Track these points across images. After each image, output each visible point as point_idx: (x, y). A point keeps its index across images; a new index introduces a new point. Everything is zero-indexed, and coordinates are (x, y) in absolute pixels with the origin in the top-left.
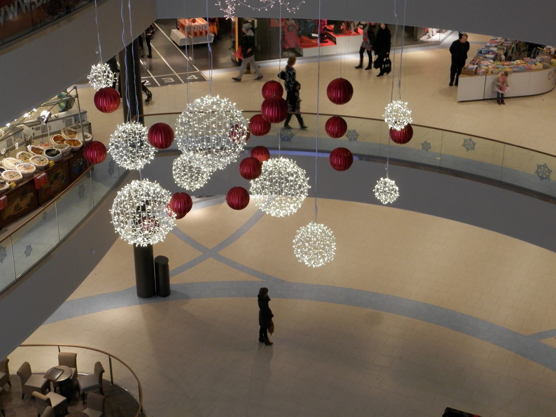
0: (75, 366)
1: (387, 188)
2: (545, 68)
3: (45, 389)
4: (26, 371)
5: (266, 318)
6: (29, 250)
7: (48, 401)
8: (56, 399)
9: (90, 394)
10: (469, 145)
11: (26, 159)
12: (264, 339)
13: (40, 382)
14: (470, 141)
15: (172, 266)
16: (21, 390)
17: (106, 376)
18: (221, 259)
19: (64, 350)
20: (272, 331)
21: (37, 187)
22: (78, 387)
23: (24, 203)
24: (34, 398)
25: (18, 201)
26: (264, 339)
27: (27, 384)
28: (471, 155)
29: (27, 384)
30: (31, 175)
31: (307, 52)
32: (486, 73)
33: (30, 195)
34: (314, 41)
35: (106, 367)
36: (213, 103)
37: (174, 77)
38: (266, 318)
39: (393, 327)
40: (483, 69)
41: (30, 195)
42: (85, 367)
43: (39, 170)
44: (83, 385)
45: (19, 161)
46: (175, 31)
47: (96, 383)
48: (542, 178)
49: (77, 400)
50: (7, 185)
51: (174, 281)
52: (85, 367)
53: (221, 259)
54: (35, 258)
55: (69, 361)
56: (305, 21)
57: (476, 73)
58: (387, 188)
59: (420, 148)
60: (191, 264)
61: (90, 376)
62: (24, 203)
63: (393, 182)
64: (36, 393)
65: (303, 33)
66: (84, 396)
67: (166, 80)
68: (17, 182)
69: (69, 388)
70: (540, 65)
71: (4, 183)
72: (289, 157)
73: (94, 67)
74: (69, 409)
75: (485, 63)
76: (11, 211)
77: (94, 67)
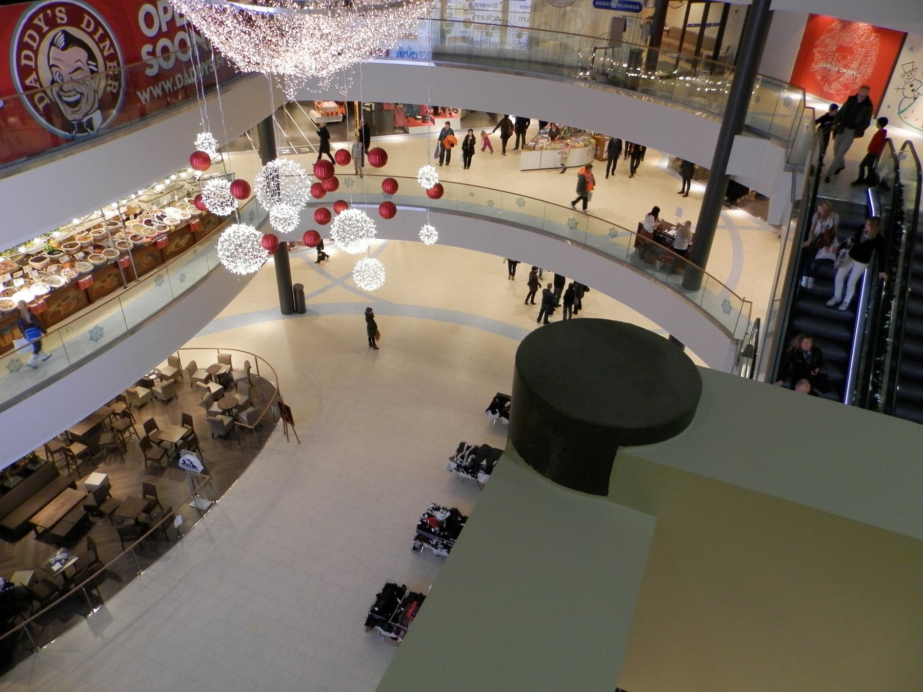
0: (230, 363)
1: (429, 234)
2: (586, 146)
3: (206, 381)
4: (193, 368)
5: (373, 331)
6: (183, 278)
7: (209, 389)
8: (215, 387)
9: (239, 384)
10: (521, 204)
11: (184, 208)
12: (373, 345)
13: (204, 375)
14: (522, 199)
15: (306, 292)
16: (189, 380)
17: (253, 371)
18: (346, 286)
19: (222, 352)
20: (378, 339)
21: (193, 230)
22: (232, 379)
23: (183, 242)
24: (198, 387)
25: (178, 240)
26: (373, 345)
27: (194, 376)
28: (522, 210)
29: (194, 376)
30: (187, 221)
31: (412, 130)
32: (541, 148)
33: (188, 236)
34: (418, 122)
35: (253, 365)
36: (283, 165)
37: (310, 148)
38: (373, 331)
39: (830, 395)
40: (540, 145)
41: (188, 236)
42: (238, 364)
43: (193, 217)
44: (235, 376)
45: (179, 210)
46: (313, 111)
47: (246, 376)
48: (571, 228)
49: (232, 388)
50: (168, 229)
51: (308, 302)
52: (238, 364)
53: (346, 286)
54: (188, 284)
55: (227, 360)
56: (411, 106)
57: (534, 148)
58: (429, 234)
59: (486, 204)
60: (322, 290)
61: (242, 371)
62: (183, 242)
63: (433, 228)
64: (199, 383)
65: (411, 116)
66: (236, 384)
67: (303, 150)
68: (176, 226)
69: (226, 381)
70: (582, 144)
71: (165, 227)
72: (362, 209)
73: (199, 135)
74: (226, 394)
75: (542, 141)
76: (172, 248)
77: (199, 135)
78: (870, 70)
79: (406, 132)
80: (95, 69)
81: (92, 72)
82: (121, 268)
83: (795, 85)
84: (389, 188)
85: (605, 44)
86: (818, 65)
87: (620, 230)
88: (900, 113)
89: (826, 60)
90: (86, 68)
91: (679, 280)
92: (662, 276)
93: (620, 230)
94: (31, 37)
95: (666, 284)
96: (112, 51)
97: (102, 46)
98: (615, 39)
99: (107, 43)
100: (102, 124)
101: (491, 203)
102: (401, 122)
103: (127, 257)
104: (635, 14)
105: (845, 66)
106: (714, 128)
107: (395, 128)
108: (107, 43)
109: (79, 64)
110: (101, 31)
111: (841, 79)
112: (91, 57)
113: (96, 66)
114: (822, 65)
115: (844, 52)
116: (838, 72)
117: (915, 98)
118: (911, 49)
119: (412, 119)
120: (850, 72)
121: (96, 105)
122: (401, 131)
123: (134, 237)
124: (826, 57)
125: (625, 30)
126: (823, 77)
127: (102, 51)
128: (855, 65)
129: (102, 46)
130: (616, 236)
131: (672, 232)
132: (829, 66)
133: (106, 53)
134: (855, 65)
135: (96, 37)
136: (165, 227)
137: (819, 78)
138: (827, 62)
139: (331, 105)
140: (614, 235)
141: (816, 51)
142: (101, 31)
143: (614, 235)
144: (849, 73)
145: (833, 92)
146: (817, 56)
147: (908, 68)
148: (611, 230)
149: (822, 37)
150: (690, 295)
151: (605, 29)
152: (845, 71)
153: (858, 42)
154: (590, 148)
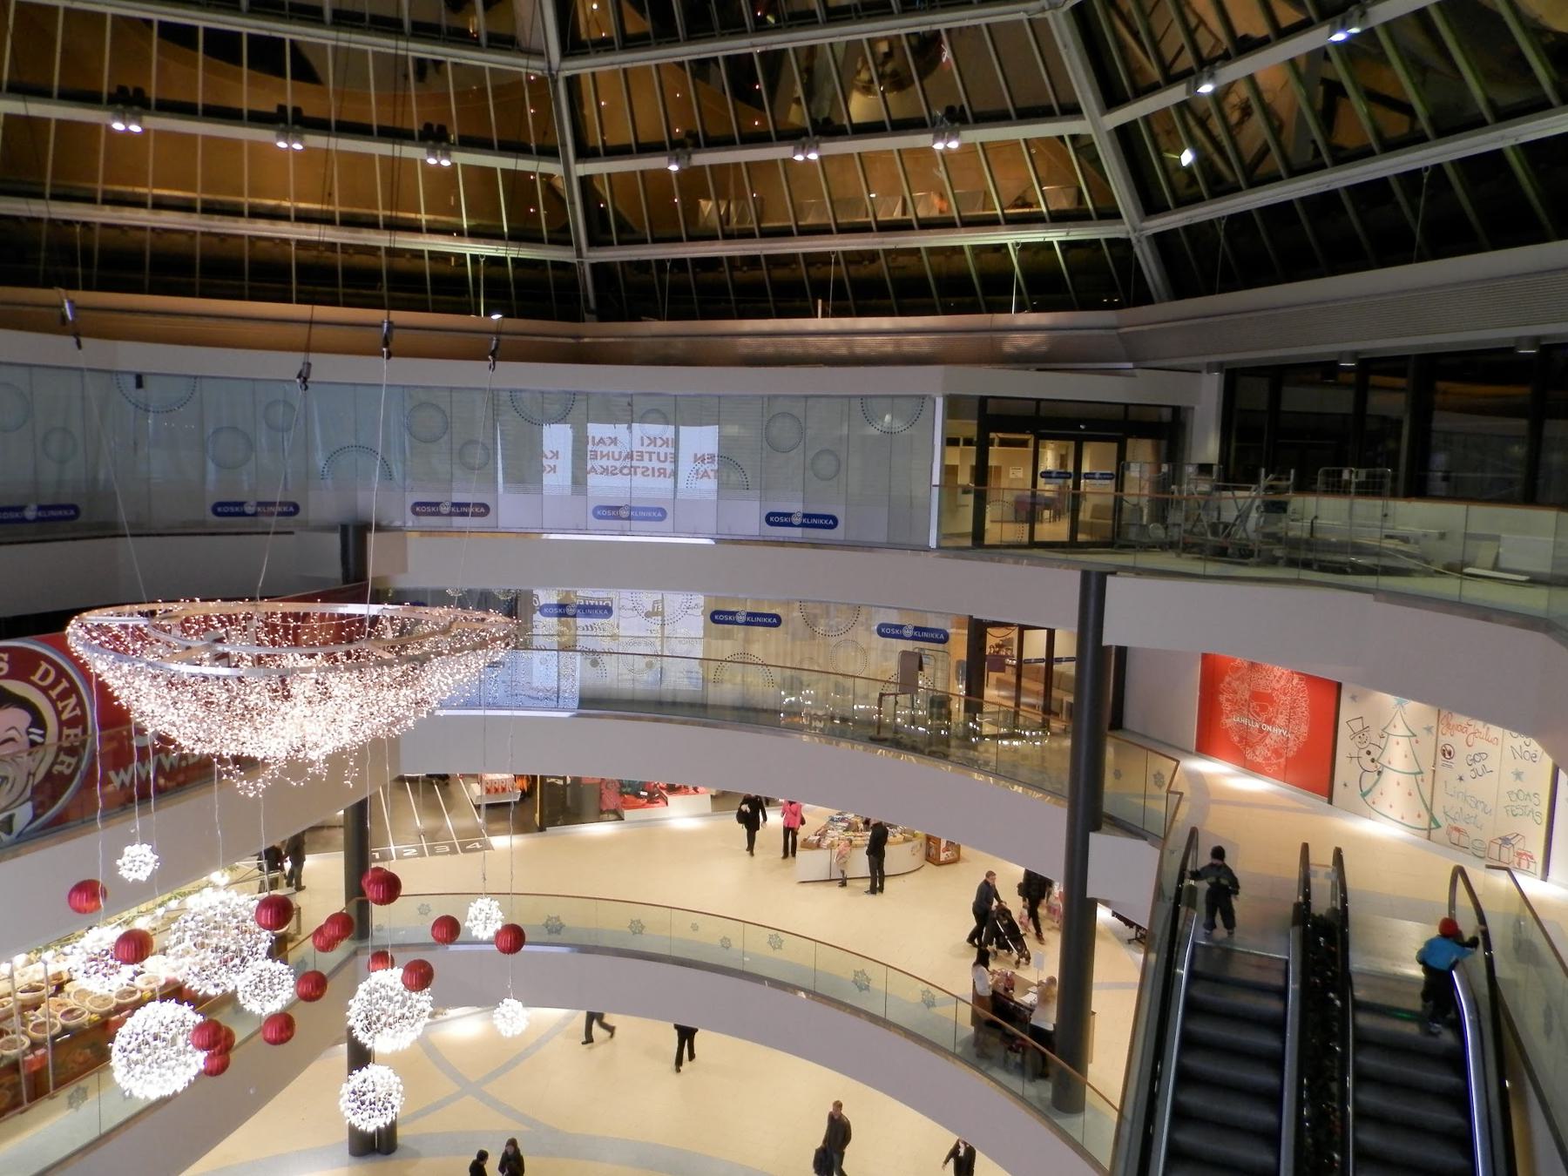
2: (906, 840)
10: (776, 944)
50: (138, 995)
57: (818, 846)
71: (134, 993)
75: (835, 833)
78: (1304, 729)
79: (621, 818)
80: (39, 740)
81: (33, 744)
82: (23, 1072)
83: (1205, 746)
84: (444, 932)
85: (893, 689)
86: (1231, 720)
87: (938, 994)
88: (1364, 795)
89: (1239, 711)
90: (25, 739)
91: (1045, 1089)
92: (1016, 1083)
93: (938, 994)
94: (46, 674)
95: (1021, 1099)
96: (78, 712)
97: (60, 705)
98: (907, 683)
99: (73, 701)
100: (31, 822)
101: (726, 944)
102: (611, 800)
103: (40, 1052)
104: (940, 647)
105: (1268, 722)
106: (1055, 818)
107: (602, 812)
108: (73, 701)
109: (12, 733)
110: (65, 684)
111: (1268, 741)
112: (38, 721)
113: (43, 736)
114: (1235, 719)
115: (1261, 701)
116: (1261, 731)
117: (1380, 773)
118: (1353, 698)
119: (632, 798)
120: (1276, 730)
121: (28, 793)
122: (612, 817)
123: (69, 1012)
124: (1239, 707)
125: (921, 668)
126: (1242, 738)
127: (58, 713)
128: (1281, 720)
129: (60, 705)
130: (933, 1005)
131: (1029, 998)
132: (1245, 721)
133: (65, 716)
134: (1281, 720)
135: (54, 694)
136: (134, 993)
137: (1236, 739)
138: (1243, 715)
139: (503, 777)
140: (930, 1003)
141: (1222, 698)
142: (65, 684)
143: (930, 1003)
144: (1276, 732)
145: (1259, 760)
146: (1226, 707)
147: (1357, 726)
148: (923, 993)
149: (1227, 679)
150: (1065, 1122)
151: (892, 667)
152: (1269, 728)
153: (1277, 686)
154: (916, 842)
